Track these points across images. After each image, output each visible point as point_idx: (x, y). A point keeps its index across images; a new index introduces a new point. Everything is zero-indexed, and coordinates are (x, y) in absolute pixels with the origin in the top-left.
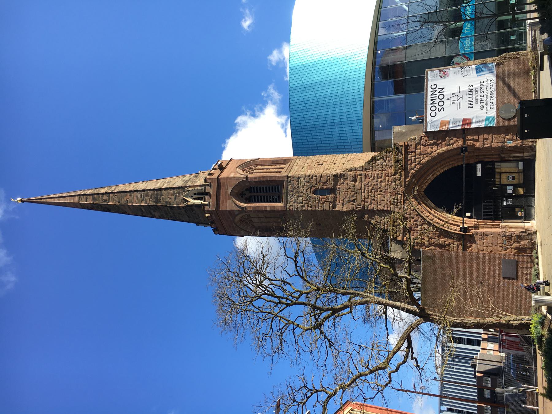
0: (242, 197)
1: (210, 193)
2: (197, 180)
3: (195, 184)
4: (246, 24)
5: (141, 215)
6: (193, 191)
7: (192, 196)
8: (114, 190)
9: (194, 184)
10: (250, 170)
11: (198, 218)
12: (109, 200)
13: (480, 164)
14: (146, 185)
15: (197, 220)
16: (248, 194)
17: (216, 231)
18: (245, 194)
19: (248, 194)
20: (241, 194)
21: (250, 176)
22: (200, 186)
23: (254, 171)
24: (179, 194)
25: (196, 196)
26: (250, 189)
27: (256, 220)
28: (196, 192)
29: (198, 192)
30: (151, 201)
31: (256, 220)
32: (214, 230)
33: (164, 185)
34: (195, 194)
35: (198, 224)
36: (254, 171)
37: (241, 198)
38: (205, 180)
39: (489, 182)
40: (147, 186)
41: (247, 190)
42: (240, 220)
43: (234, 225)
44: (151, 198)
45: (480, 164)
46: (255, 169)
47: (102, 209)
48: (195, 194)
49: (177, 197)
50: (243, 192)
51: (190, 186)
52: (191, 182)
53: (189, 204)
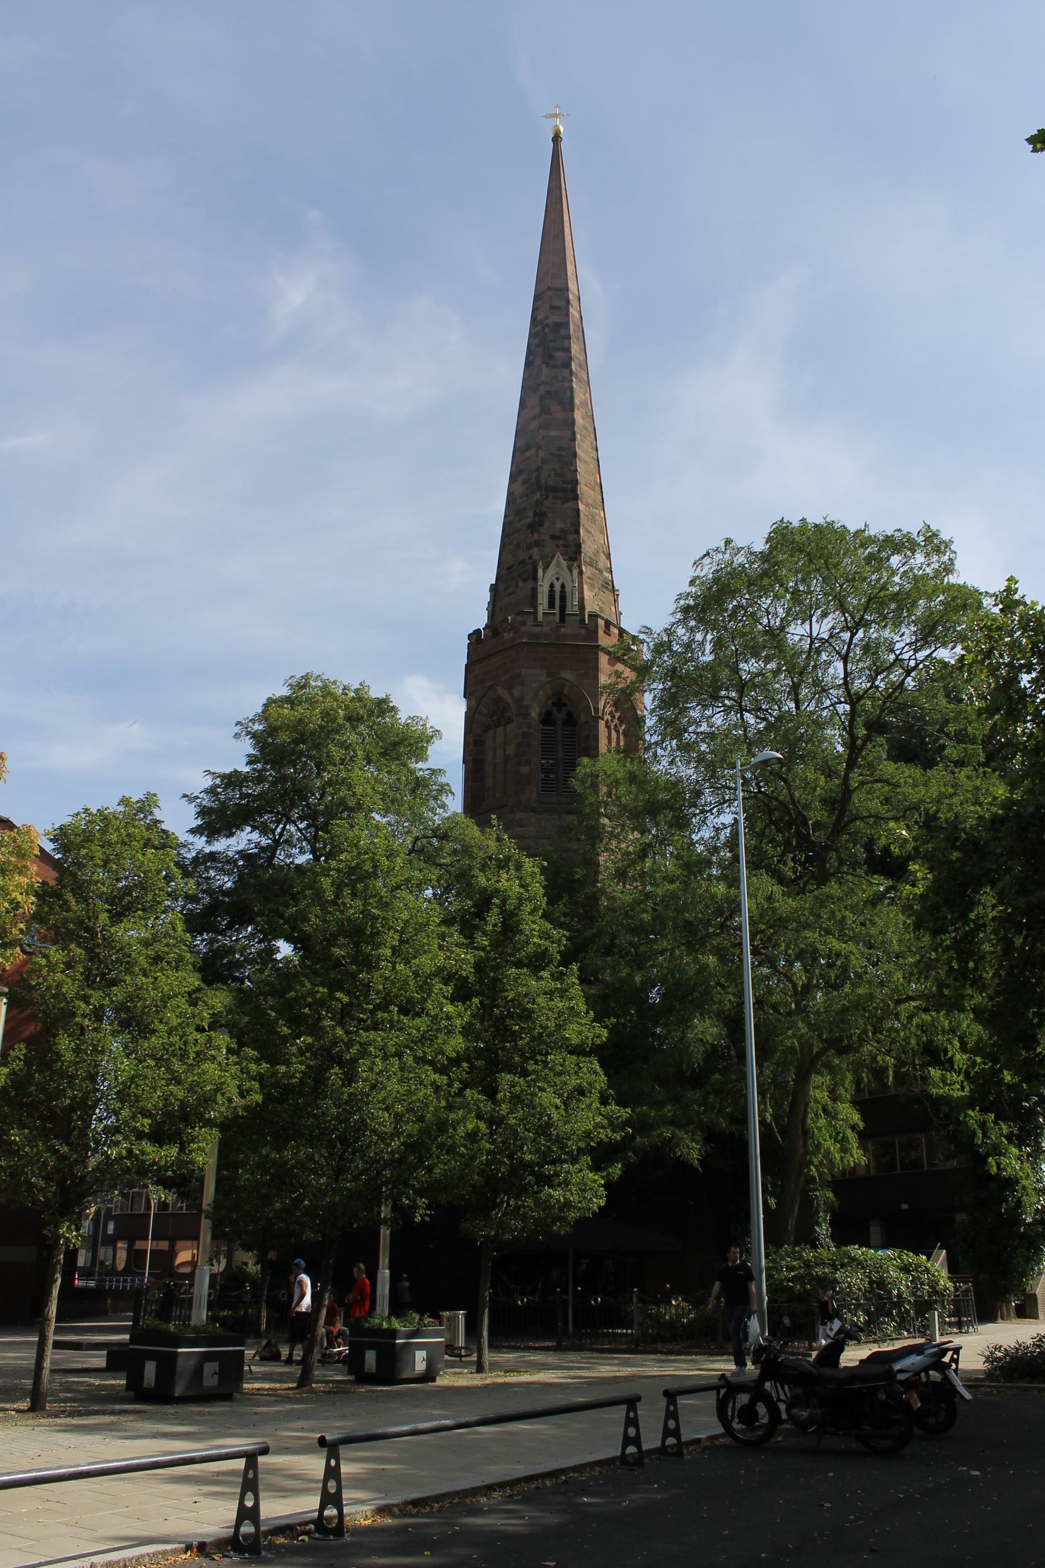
0: (554, 704)
1: (564, 627)
2: (597, 590)
3: (585, 586)
4: (727, 1532)
5: (518, 446)
6: (570, 583)
7: (558, 579)
8: (576, 377)
9: (587, 583)
10: (616, 721)
11: (508, 591)
12: (554, 366)
13: (145, 1385)
14: (588, 459)
15: (501, 588)
16: (560, 717)
17: (475, 636)
18: (559, 711)
19: (560, 717)
20: (559, 700)
21: (602, 724)
22: (582, 600)
23: (613, 732)
24: (565, 546)
25: (557, 589)
26: (570, 720)
27: (500, 739)
28: (568, 589)
29: (568, 595)
30: (549, 476)
31: (500, 739)
32: (477, 632)
33: (587, 505)
34: (563, 586)
35: (494, 589)
36: (613, 732)
37: (550, 702)
38: (594, 616)
39: (731, 1404)
40: (585, 462)
41: (570, 715)
42: (500, 699)
43: (489, 684)
44: (557, 475)
45: (145, 1385)
46: (617, 732)
47: (532, 348)
48: (563, 586)
49: (557, 542)
50: (565, 705)
51: (581, 573)
52: (592, 574)
53: (540, 572)
